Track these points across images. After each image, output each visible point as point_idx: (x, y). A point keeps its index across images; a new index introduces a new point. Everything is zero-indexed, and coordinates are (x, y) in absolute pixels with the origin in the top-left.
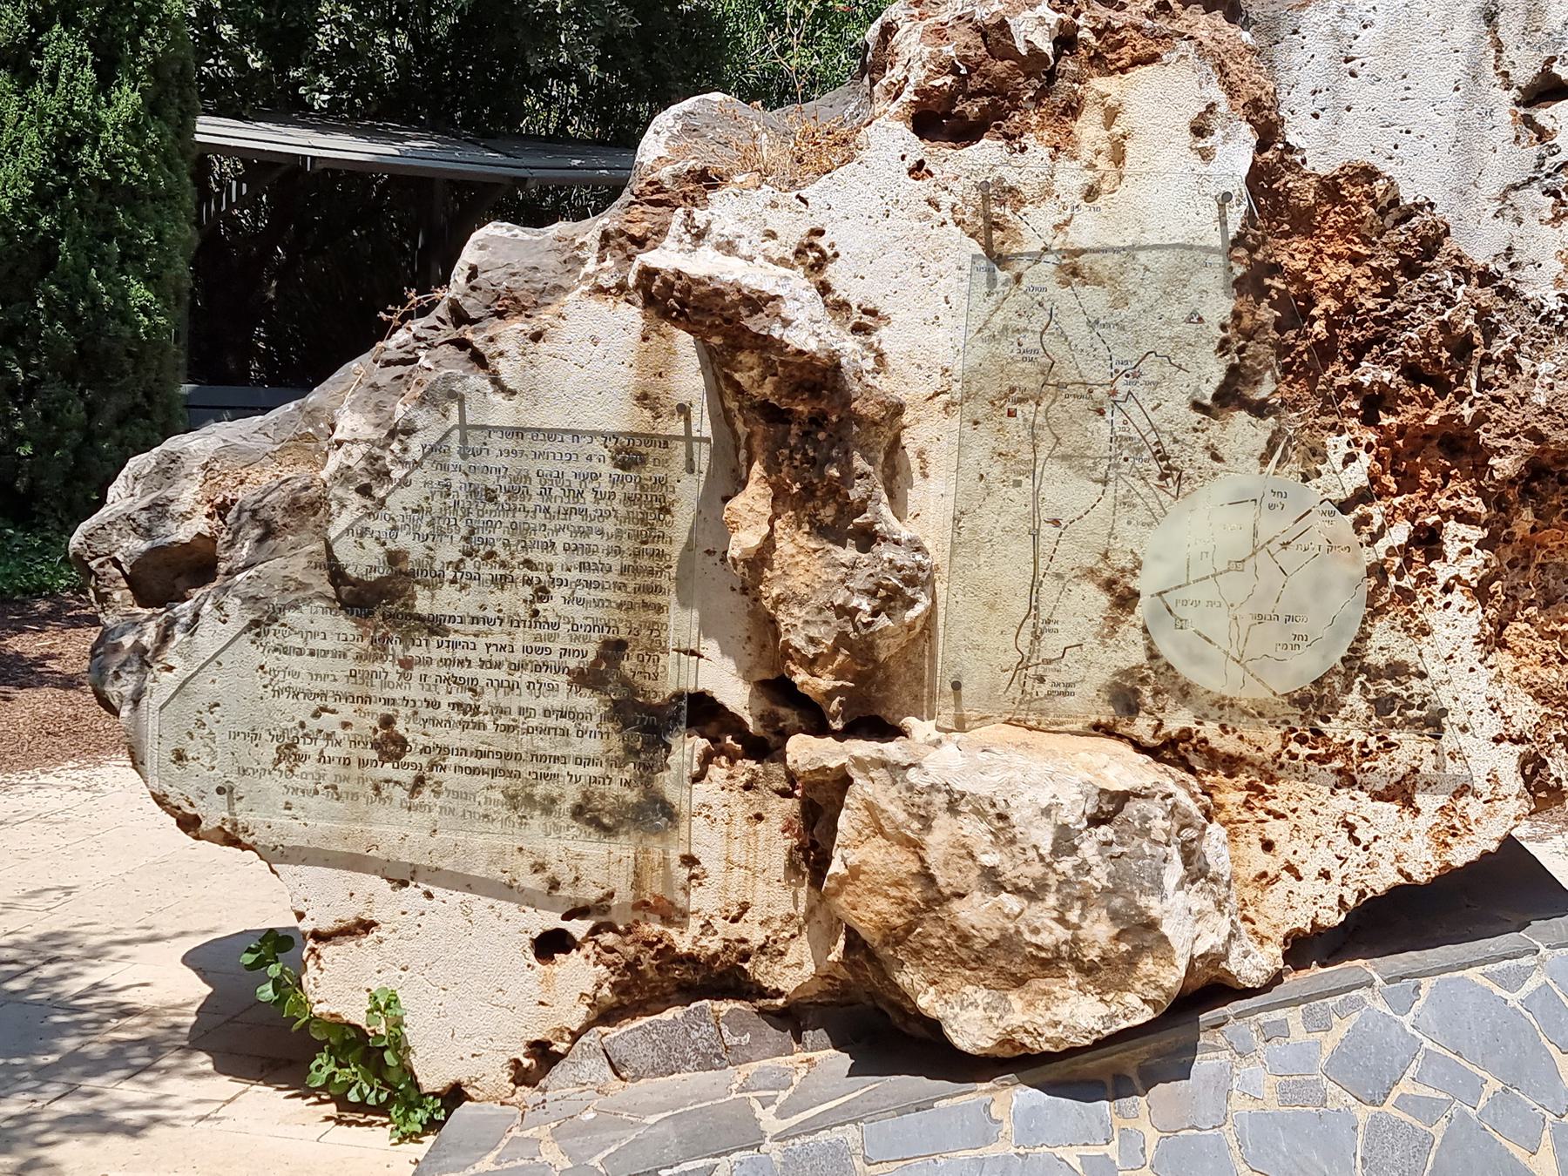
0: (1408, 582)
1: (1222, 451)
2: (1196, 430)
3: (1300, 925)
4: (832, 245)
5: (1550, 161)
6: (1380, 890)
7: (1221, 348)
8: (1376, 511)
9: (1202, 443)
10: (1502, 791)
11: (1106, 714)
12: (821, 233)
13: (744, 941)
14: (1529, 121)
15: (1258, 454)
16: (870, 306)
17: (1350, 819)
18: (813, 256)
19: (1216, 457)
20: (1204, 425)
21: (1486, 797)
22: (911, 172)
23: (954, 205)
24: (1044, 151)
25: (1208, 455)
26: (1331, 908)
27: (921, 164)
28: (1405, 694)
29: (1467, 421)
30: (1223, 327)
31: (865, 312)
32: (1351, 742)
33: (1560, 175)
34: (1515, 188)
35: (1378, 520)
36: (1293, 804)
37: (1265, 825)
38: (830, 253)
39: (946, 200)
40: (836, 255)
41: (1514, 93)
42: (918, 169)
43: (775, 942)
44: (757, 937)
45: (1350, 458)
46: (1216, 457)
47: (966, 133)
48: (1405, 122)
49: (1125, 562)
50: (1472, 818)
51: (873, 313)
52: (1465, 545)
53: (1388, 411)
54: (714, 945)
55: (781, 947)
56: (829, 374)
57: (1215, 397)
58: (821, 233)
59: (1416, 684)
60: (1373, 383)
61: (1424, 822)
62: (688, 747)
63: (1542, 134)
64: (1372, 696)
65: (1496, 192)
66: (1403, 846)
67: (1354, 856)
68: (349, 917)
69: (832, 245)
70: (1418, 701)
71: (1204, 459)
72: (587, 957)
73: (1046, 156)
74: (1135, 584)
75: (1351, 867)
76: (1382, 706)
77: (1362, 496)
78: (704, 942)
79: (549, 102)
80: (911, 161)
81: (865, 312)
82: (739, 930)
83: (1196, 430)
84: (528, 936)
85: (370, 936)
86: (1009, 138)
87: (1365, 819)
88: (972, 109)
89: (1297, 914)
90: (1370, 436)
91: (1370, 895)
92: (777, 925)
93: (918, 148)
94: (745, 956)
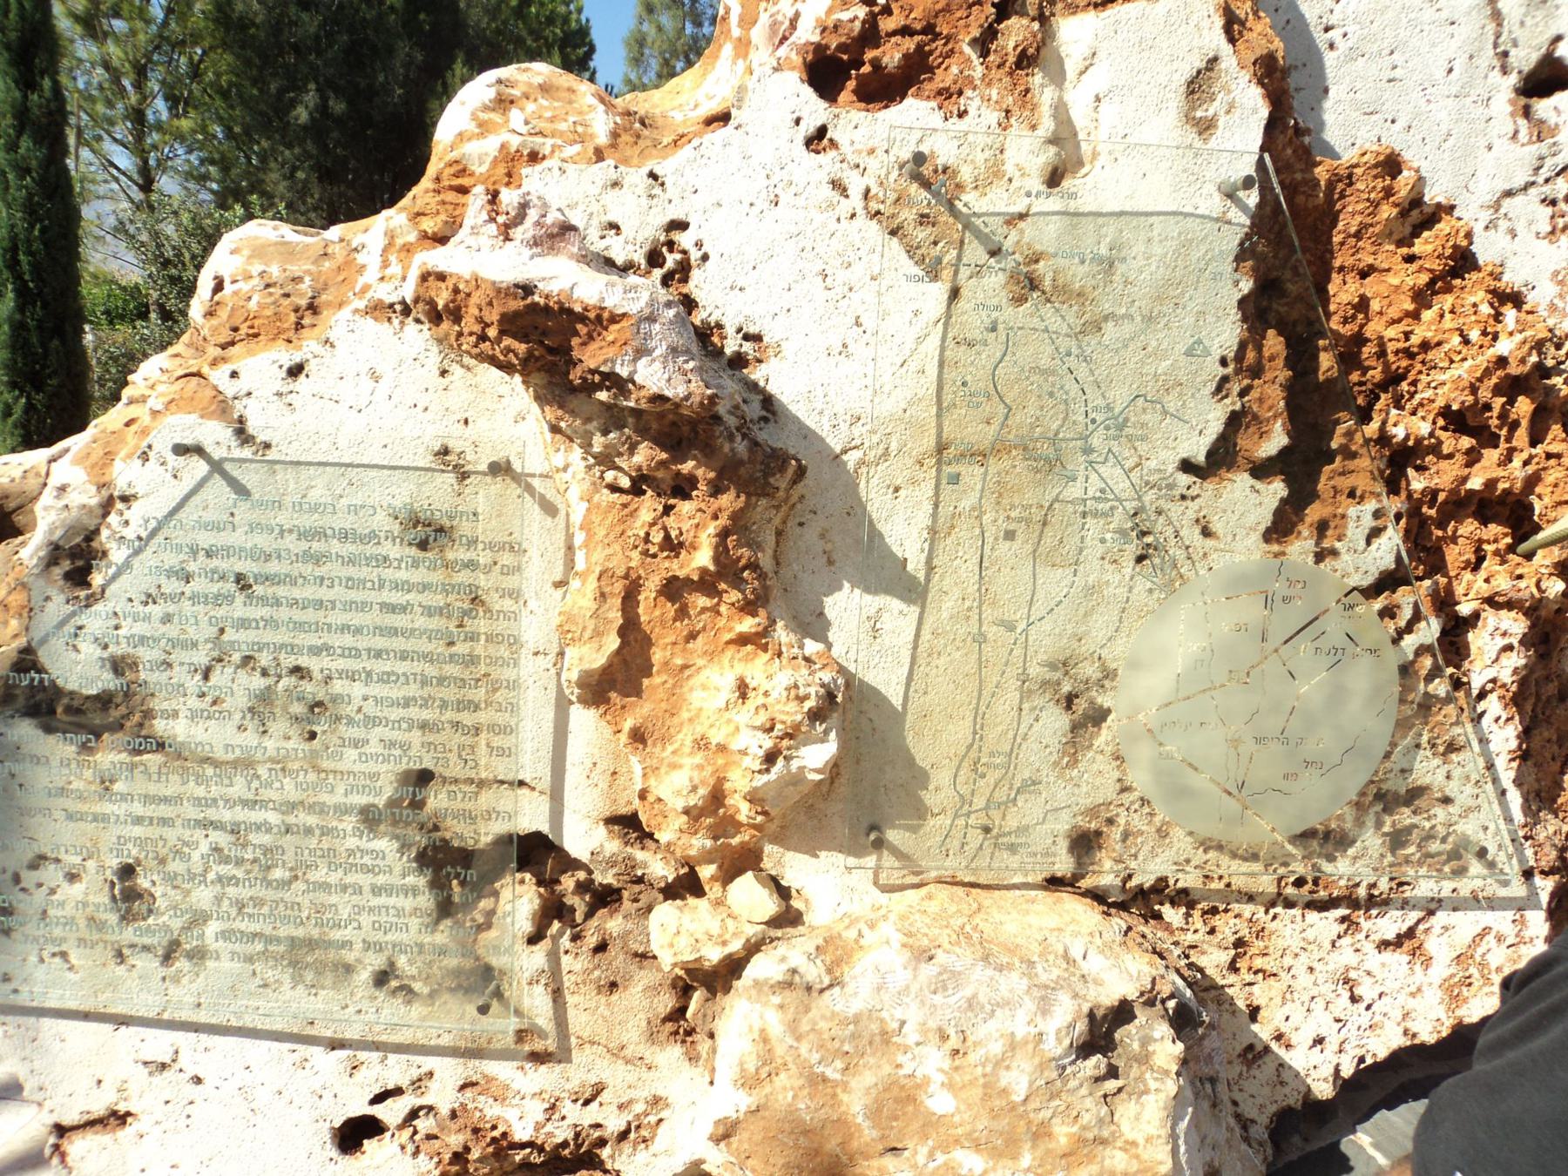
0: (1440, 687)
1: (1217, 526)
2: (1183, 497)
3: (1291, 1102)
4: (699, 245)
5: (1549, 162)
6: (1382, 1054)
7: (1219, 389)
8: (1405, 598)
9: (1191, 514)
10: (1527, 934)
11: (1063, 865)
12: (681, 226)
13: (598, 1126)
14: (1527, 112)
15: (1262, 528)
16: (753, 330)
17: (1353, 975)
18: (669, 260)
19: (1206, 533)
20: (1194, 491)
21: (1510, 941)
22: (809, 142)
23: (868, 191)
24: (993, 117)
25: (1197, 530)
26: (1325, 1080)
27: (822, 132)
28: (1427, 825)
29: (1411, 472)
30: (1224, 362)
31: (747, 337)
32: (1358, 885)
33: (1560, 180)
34: (1509, 194)
35: (1406, 613)
36: (1288, 961)
37: (1255, 988)
38: (695, 255)
39: (856, 185)
40: (705, 258)
41: (1513, 79)
42: (818, 139)
43: (638, 1127)
44: (614, 1123)
45: (1375, 533)
46: (1206, 533)
47: (883, 90)
48: (1388, 111)
49: (1090, 670)
50: (1493, 968)
51: (757, 338)
52: (1506, 641)
53: (1421, 469)
54: (562, 1133)
55: (645, 1133)
56: (701, 427)
57: (1210, 454)
58: (681, 226)
59: (1440, 812)
60: (1407, 437)
61: (1442, 968)
62: (519, 900)
63: (1542, 131)
64: (1386, 829)
65: (1489, 198)
66: (1411, 1003)
67: (1355, 1017)
68: (98, 1109)
69: (699, 245)
70: (1441, 831)
71: (1192, 535)
72: (403, 1148)
73: (994, 124)
74: (1104, 700)
75: (1350, 1031)
76: (1397, 840)
77: (1389, 581)
78: (549, 1128)
79: (471, 334)
80: (808, 127)
81: (747, 337)
82: (591, 1114)
83: (1183, 497)
84: (328, 1125)
85: (128, 1129)
86: (945, 94)
87: (1369, 973)
88: (892, 55)
89: (1287, 1090)
90: (1395, 504)
91: (1369, 1061)
92: (639, 1108)
93: (815, 110)
94: (602, 1142)
